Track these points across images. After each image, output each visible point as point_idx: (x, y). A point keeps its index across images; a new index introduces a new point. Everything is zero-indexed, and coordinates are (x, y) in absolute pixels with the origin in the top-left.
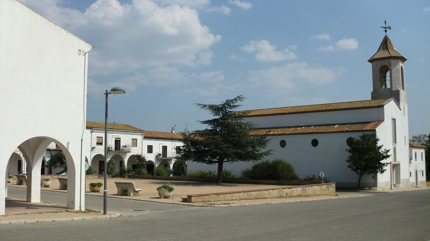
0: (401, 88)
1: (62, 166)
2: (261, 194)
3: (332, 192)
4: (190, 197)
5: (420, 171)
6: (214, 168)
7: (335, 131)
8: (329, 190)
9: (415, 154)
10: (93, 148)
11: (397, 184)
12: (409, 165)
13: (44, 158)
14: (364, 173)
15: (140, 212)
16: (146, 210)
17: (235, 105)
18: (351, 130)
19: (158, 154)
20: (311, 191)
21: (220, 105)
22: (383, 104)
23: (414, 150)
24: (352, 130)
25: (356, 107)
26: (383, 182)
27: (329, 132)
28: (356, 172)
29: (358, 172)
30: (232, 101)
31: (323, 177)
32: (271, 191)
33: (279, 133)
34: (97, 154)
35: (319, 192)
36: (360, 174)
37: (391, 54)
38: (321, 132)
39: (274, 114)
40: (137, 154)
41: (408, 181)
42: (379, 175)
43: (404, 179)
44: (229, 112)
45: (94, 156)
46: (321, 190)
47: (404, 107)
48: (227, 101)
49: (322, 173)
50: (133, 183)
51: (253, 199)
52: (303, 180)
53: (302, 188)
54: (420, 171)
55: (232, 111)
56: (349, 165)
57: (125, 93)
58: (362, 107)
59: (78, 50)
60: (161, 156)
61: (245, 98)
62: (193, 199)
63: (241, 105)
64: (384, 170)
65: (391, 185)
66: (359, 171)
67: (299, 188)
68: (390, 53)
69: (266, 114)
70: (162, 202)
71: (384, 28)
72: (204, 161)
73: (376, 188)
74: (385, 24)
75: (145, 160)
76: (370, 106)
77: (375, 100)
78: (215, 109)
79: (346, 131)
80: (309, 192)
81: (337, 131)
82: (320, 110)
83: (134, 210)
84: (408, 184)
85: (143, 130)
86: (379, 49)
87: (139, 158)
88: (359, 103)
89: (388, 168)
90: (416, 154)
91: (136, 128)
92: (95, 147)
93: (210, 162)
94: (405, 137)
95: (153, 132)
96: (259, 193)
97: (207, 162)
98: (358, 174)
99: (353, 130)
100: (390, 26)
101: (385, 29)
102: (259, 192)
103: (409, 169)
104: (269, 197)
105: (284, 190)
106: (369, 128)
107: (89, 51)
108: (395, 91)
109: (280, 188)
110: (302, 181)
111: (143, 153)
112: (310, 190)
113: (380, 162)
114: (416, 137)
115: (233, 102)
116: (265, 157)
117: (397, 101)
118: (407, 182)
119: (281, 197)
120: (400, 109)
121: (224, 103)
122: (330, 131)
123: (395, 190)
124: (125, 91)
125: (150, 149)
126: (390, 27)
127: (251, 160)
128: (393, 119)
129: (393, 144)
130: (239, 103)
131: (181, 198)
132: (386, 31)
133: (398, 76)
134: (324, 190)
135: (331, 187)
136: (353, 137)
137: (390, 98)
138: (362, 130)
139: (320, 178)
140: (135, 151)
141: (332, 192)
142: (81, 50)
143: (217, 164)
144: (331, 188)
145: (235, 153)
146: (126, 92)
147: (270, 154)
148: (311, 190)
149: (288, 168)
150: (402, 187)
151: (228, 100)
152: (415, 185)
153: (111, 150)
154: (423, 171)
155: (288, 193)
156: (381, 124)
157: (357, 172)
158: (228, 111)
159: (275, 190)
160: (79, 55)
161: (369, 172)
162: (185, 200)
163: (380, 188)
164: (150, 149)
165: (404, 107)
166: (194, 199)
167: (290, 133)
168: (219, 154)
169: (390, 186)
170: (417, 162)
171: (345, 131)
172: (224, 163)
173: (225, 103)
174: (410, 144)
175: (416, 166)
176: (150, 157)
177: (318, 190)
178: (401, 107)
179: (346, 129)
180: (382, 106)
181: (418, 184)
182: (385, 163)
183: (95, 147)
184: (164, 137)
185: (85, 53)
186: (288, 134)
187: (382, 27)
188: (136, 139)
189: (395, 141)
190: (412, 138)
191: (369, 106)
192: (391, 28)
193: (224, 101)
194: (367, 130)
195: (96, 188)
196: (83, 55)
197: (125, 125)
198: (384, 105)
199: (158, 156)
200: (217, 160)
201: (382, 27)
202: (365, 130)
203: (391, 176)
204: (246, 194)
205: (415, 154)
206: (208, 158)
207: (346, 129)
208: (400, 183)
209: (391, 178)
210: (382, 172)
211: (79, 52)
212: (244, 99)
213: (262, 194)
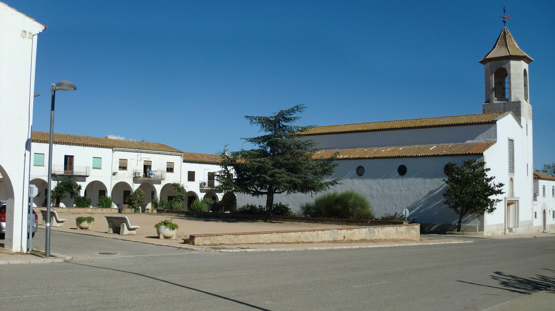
0: (524, 99)
1: (73, 197)
2: (304, 237)
3: (415, 236)
4: (192, 237)
5: (550, 211)
6: (261, 201)
7: (429, 155)
8: (409, 234)
9: (542, 188)
10: (114, 174)
11: (514, 227)
12: (533, 203)
14: (466, 212)
15: (106, 256)
16: (117, 254)
17: (292, 118)
18: (451, 154)
19: (202, 182)
20: (382, 233)
21: (271, 117)
22: (496, 119)
23: (541, 183)
24: (452, 154)
25: (460, 123)
26: (493, 225)
27: (421, 156)
28: (455, 209)
29: (457, 211)
30: (288, 112)
31: (407, 216)
32: (320, 232)
33: (356, 157)
34: (119, 182)
35: (395, 236)
36: (460, 213)
37: (510, 53)
38: (411, 155)
39: (351, 131)
40: (173, 183)
41: (530, 224)
42: (487, 216)
43: (524, 221)
44: (283, 127)
45: (116, 185)
46: (397, 232)
47: (527, 124)
48: (280, 112)
49: (406, 210)
50: (126, 217)
51: (291, 243)
52: (379, 219)
53: (369, 230)
54: (550, 211)
55: (287, 126)
56: (446, 200)
57: (75, 89)
58: (467, 123)
59: (22, 31)
60: (207, 185)
61: (305, 108)
62: (196, 240)
63: (299, 118)
64: (493, 209)
65: (505, 229)
66: (459, 209)
67: (364, 229)
68: (509, 51)
69: (341, 132)
70: (155, 243)
72: (248, 192)
73: (482, 232)
74: (504, 12)
75: (184, 190)
76: (478, 122)
77: (487, 114)
78: (266, 122)
79: (443, 154)
80: (379, 235)
81: (432, 155)
82: (411, 127)
83: (100, 252)
84: (530, 228)
85: (182, 151)
86: (495, 45)
87: (176, 187)
88: (465, 118)
89: (500, 207)
90: (544, 188)
91: (173, 149)
92: (117, 173)
93: (257, 193)
94: (527, 164)
95: (196, 155)
96: (301, 235)
97: (252, 193)
98: (458, 212)
99: (453, 154)
102: (300, 233)
103: (532, 209)
104: (316, 241)
105: (339, 231)
106: (475, 152)
107: (39, 33)
108: (515, 102)
109: (334, 229)
110: (378, 220)
111: (181, 181)
112: (380, 232)
114: (549, 167)
115: (290, 114)
116: (331, 187)
117: (518, 115)
118: (529, 225)
119: (335, 241)
120: (522, 127)
121: (276, 115)
122: (423, 155)
123: (509, 235)
124: (76, 87)
125: (191, 176)
127: (310, 192)
128: (510, 140)
129: (510, 174)
130: (297, 114)
131: (182, 239)
133: (519, 83)
134: (402, 233)
135: (413, 229)
136: (452, 162)
137: (507, 112)
138: (464, 153)
139: (403, 217)
140: (170, 178)
141: (415, 236)
142: (26, 31)
143: (265, 196)
144: (413, 231)
145: (289, 182)
146: (77, 89)
147: (337, 183)
148: (382, 233)
149: (361, 203)
150: (520, 231)
151: (282, 111)
152: (542, 230)
153: (138, 176)
155: (346, 236)
156: (492, 146)
157: (456, 211)
158: (282, 125)
159: (326, 232)
160: (23, 38)
161: (472, 210)
162: (186, 242)
163: (488, 233)
164: (191, 176)
165: (527, 124)
166: (198, 240)
167: (369, 157)
168: (268, 183)
169: (504, 230)
170: (546, 199)
171: (442, 154)
172: (274, 194)
173: (277, 115)
174: (534, 174)
175: (544, 204)
176: (192, 187)
177: (393, 234)
178: (522, 124)
179: (444, 152)
180: (494, 122)
181: (546, 229)
182: (495, 199)
183: (117, 173)
184: (210, 160)
185: (33, 36)
186: (367, 158)
188: (173, 163)
189: (512, 169)
190: (544, 168)
191: (476, 122)
193: (277, 112)
194: (471, 153)
195: (85, 224)
196: (29, 38)
197: (160, 144)
198: (497, 120)
199: (202, 186)
200: (266, 191)
202: (469, 153)
203: (505, 217)
204: (281, 236)
205: (543, 188)
206: (255, 188)
207: (444, 152)
208: (518, 227)
209: (505, 219)
210: (492, 210)
211: (23, 34)
212: (304, 109)
213: (305, 236)
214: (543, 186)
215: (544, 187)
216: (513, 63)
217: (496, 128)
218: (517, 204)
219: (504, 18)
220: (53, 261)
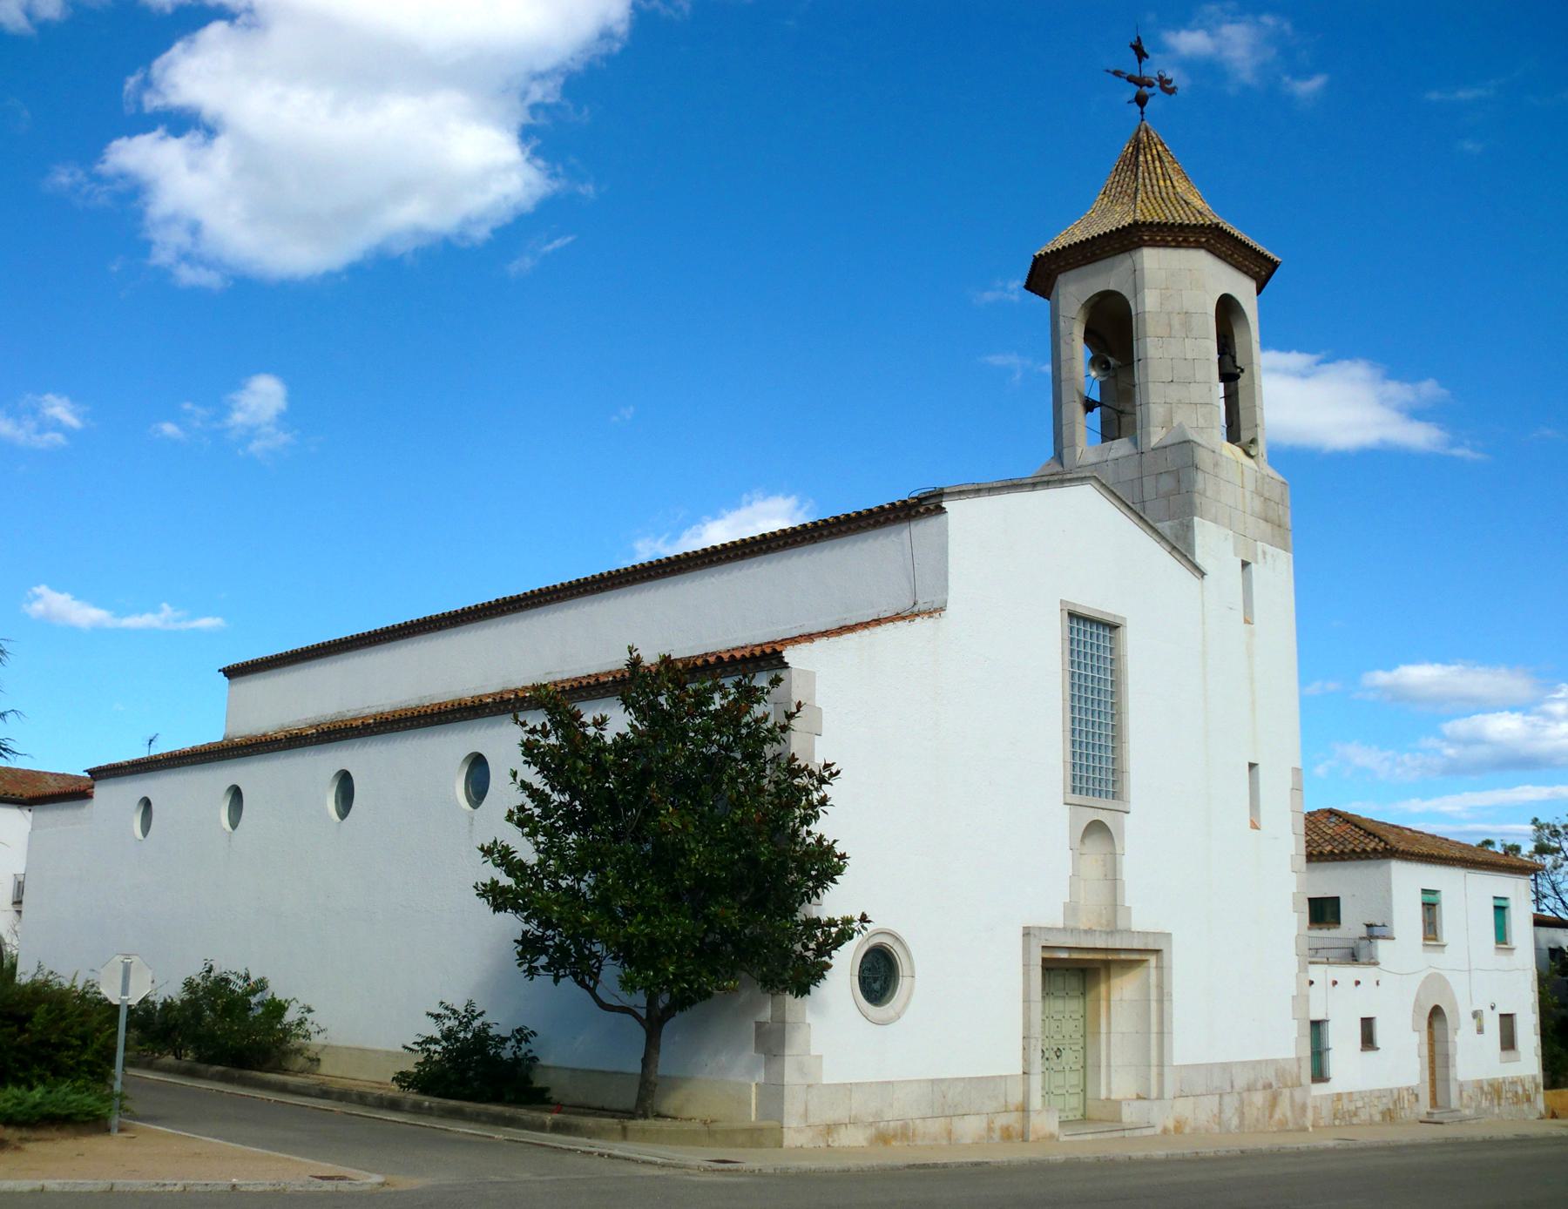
13: (475, 794)
71: (1130, 79)
100: (1168, 77)
101: (1136, 88)
103: (1301, 1000)
113: (540, 142)
126: (1170, 82)
128: (1072, 615)
129: (1076, 799)
132: (1141, 101)
152: (1424, 1106)
154: (1507, 1020)
187: (1117, 73)
192: (1175, 88)
201: (1117, 73)
214: (1425, 891)
215: (1431, 898)
216: (1152, 259)
217: (944, 533)
218: (1153, 972)
219: (1136, 83)
220: (337, 1187)
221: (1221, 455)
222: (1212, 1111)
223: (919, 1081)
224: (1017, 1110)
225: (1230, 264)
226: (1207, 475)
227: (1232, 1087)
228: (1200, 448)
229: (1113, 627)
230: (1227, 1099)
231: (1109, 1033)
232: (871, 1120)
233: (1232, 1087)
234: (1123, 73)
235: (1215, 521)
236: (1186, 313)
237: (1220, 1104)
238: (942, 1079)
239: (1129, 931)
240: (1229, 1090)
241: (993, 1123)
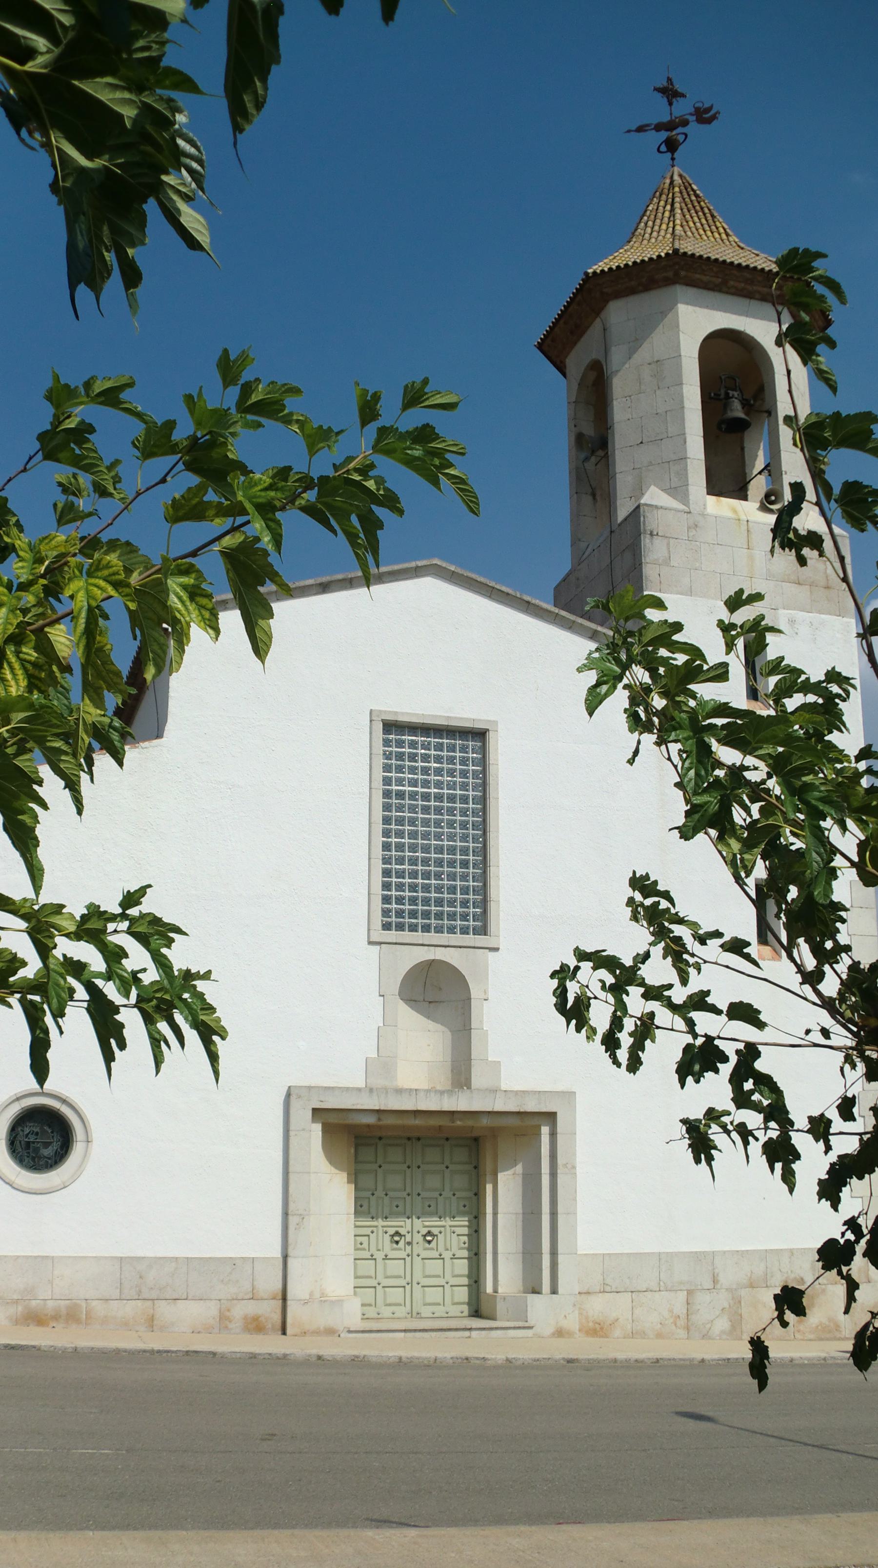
128: (390, 726)
129: (393, 935)
221: (703, 515)
222: (671, 1311)
223: (97, 1259)
224: (274, 1298)
225: (727, 293)
226: (672, 541)
227: (715, 1281)
228: (660, 512)
229: (480, 735)
230: (703, 1299)
231: (495, 1214)
232: (15, 1297)
233: (715, 1281)
234: (648, 125)
235: (690, 592)
236: (658, 361)
237: (688, 1304)
238: (139, 1258)
239: (494, 1091)
240: (708, 1284)
241: (229, 1310)
